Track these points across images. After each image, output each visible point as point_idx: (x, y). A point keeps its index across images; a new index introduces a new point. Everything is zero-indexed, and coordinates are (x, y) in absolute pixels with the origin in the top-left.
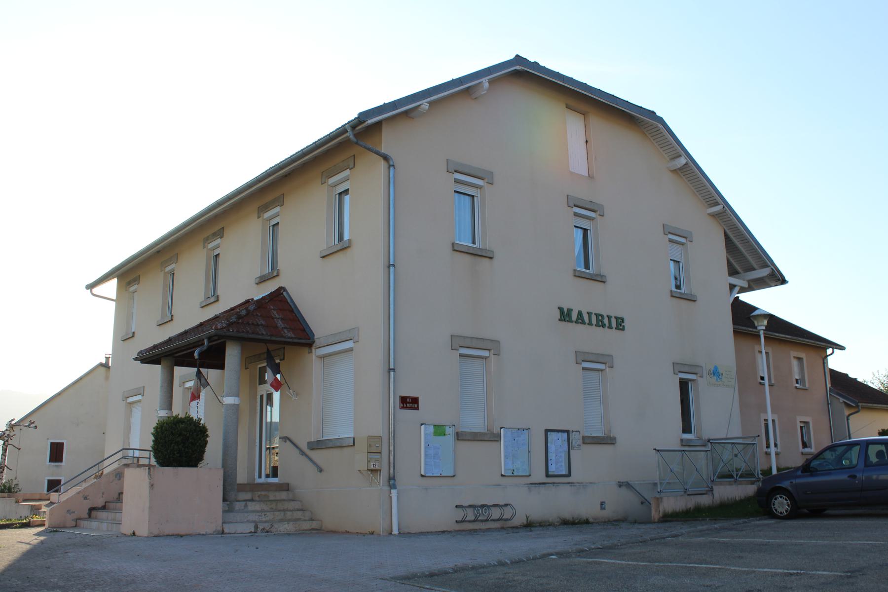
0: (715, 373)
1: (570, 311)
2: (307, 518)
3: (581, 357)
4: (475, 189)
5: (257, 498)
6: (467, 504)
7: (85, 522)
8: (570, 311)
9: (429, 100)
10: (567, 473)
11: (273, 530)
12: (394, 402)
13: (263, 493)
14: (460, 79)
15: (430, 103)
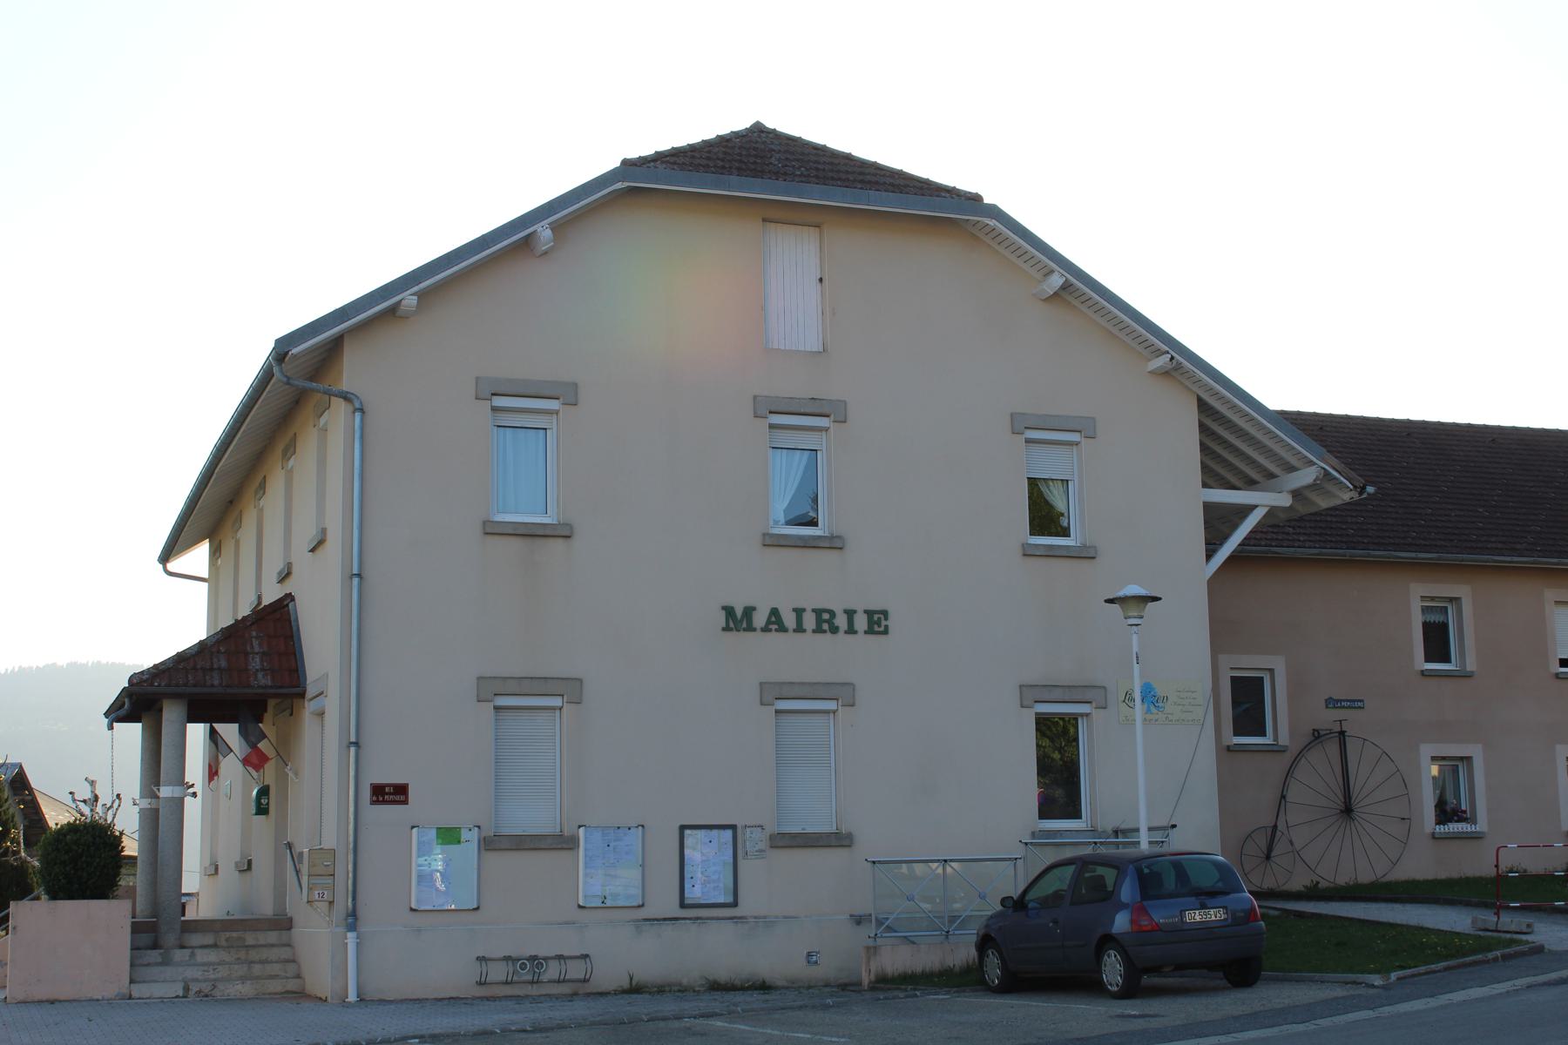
0: (1151, 697)
1: (749, 611)
2: (551, 963)
3: (772, 692)
4: (816, 435)
5: (224, 943)
6: (553, 954)
7: (156, 970)
8: (749, 611)
9: (416, 289)
10: (730, 899)
11: (217, 993)
12: (366, 793)
13: (234, 934)
14: (1114, 296)
15: (421, 295)
